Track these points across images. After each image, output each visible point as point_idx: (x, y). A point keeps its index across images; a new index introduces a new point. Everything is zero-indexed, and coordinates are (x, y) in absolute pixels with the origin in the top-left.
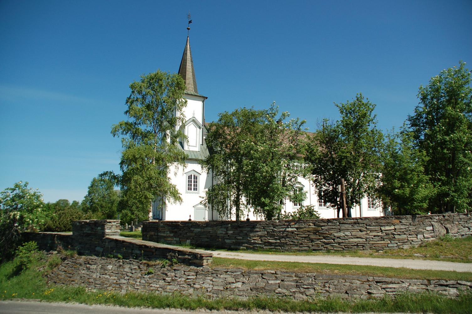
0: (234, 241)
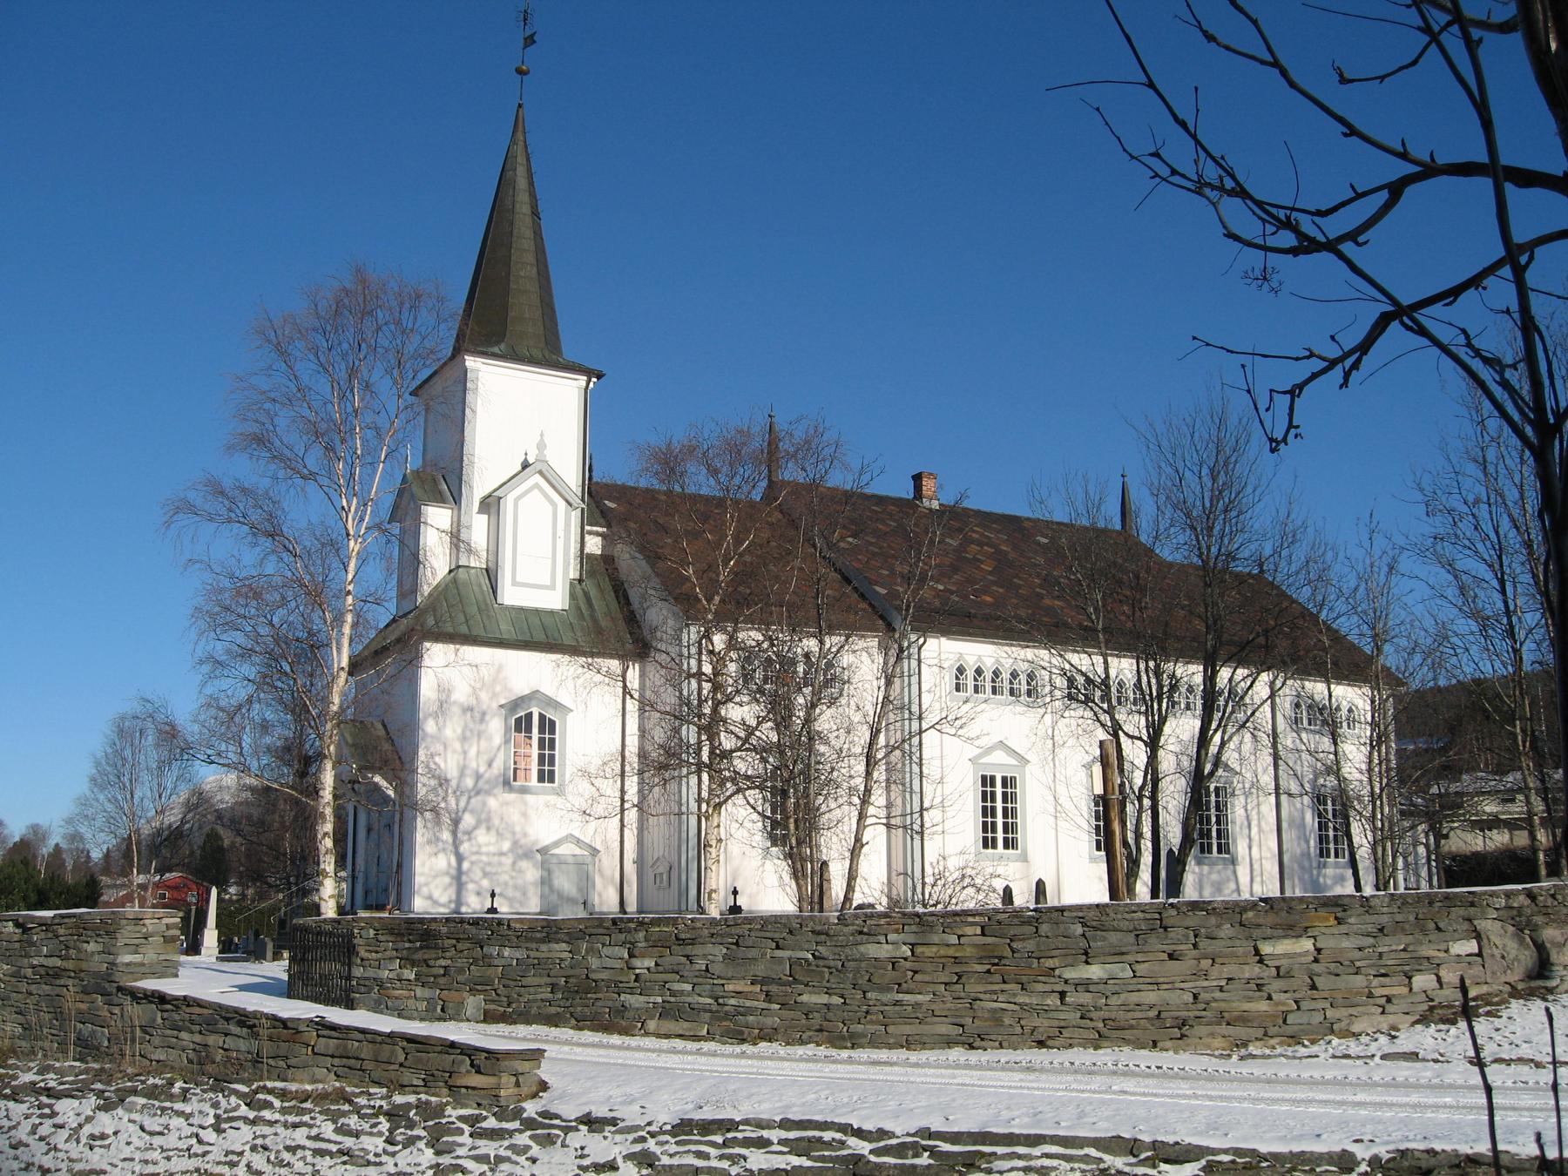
0: (659, 1000)
